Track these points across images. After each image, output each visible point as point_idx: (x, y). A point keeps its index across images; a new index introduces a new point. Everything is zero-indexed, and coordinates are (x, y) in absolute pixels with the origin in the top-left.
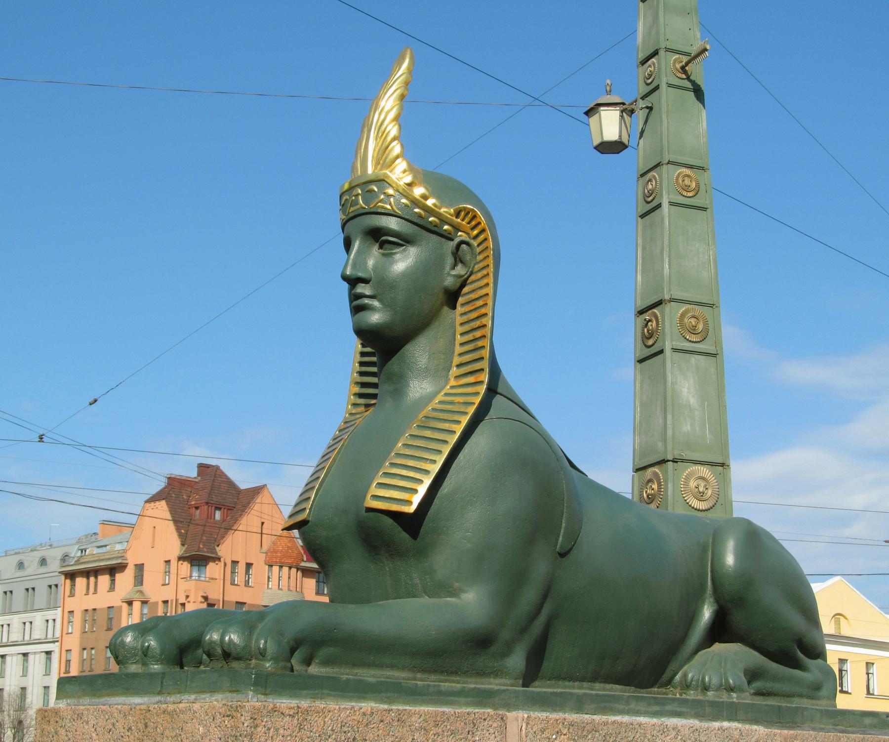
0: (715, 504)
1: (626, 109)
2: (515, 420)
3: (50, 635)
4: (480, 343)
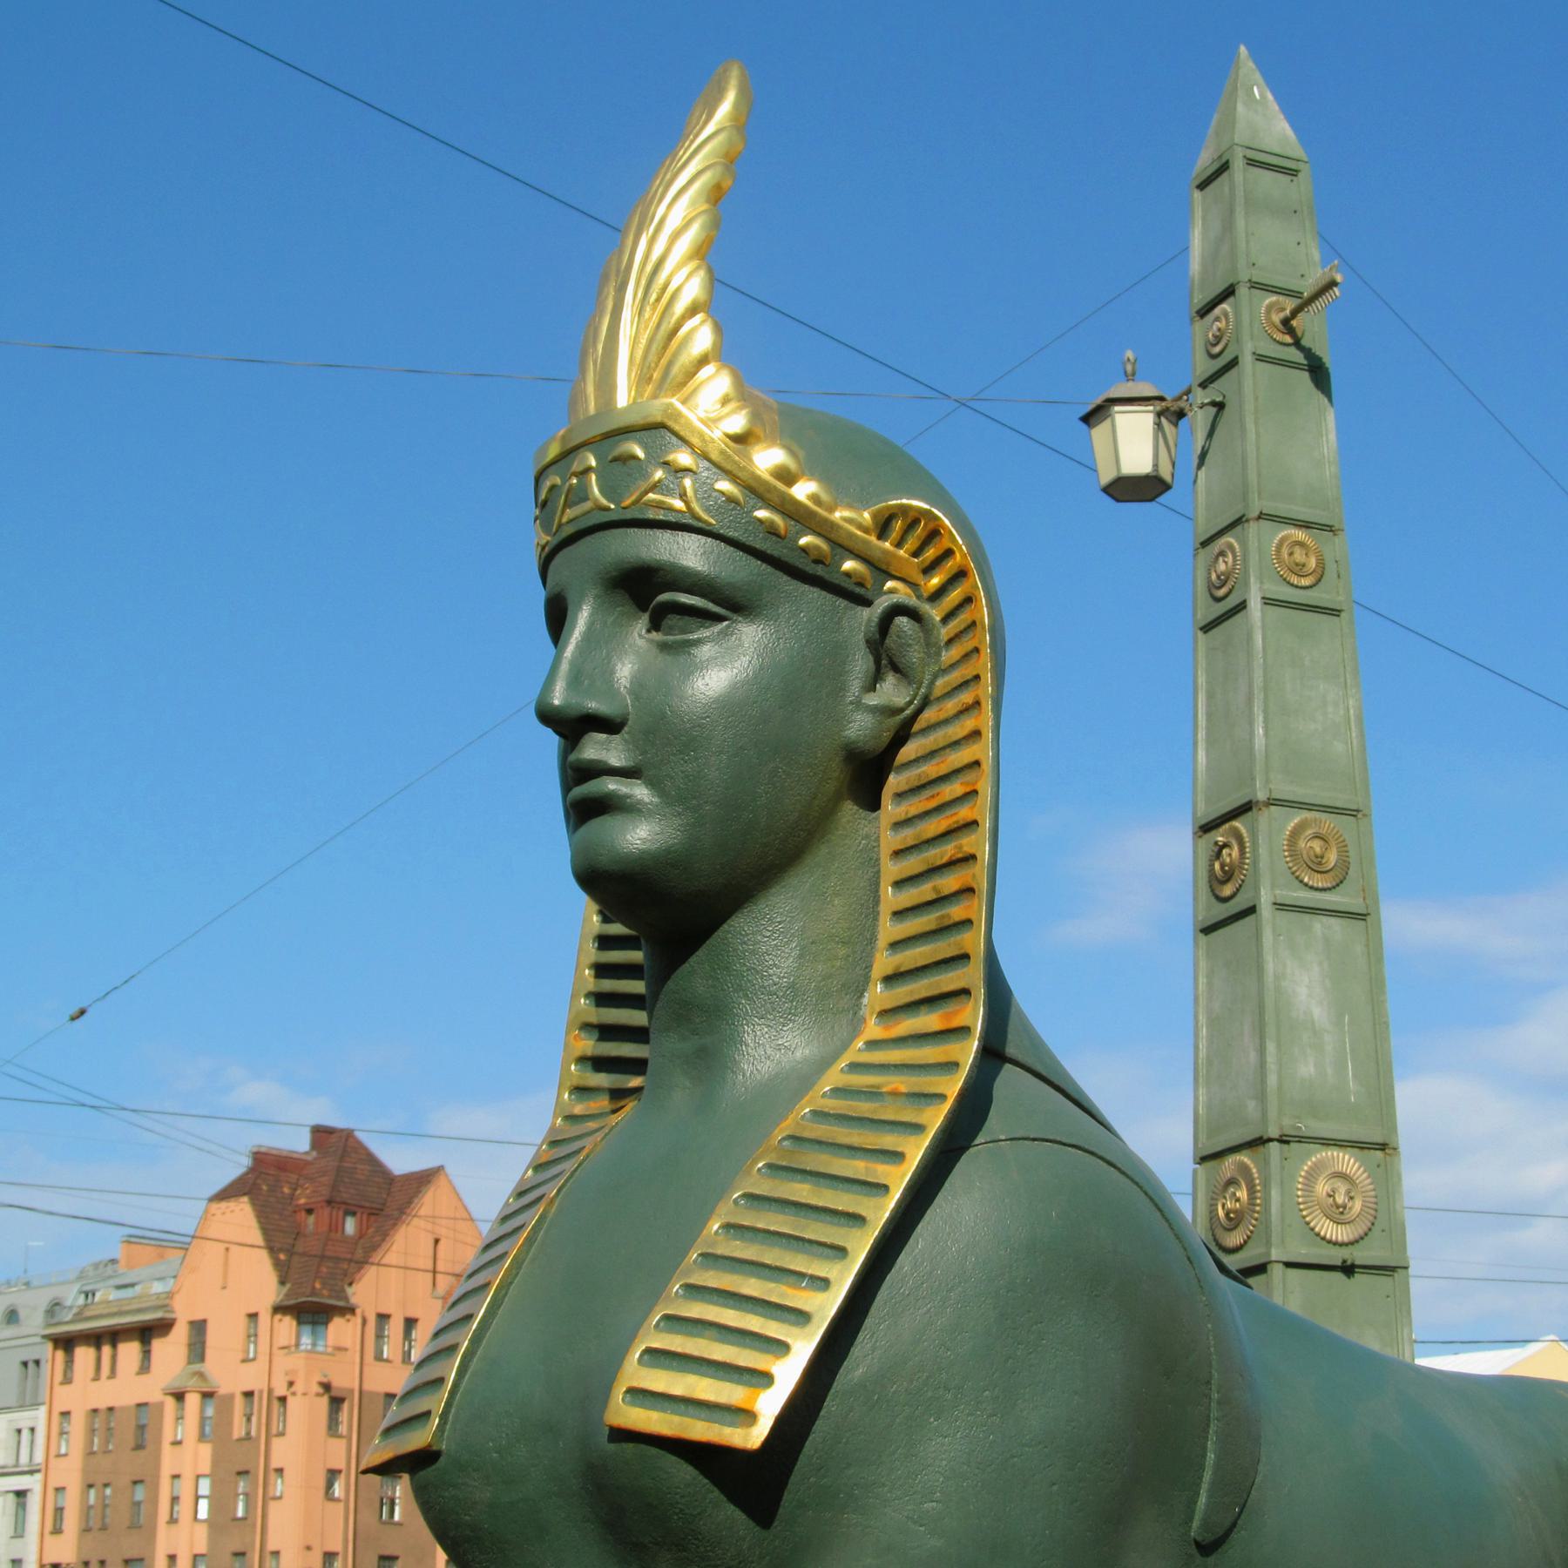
0: (1370, 1229)
1: (1167, 409)
2: (1064, 1144)
3: (24, 1459)
4: (956, 912)
